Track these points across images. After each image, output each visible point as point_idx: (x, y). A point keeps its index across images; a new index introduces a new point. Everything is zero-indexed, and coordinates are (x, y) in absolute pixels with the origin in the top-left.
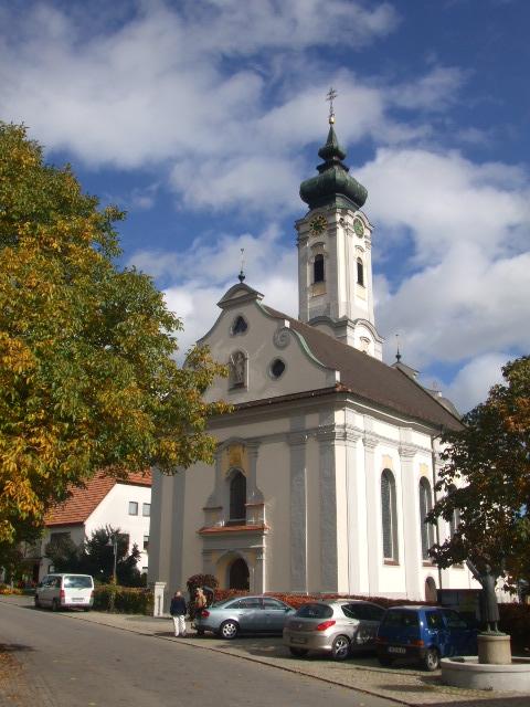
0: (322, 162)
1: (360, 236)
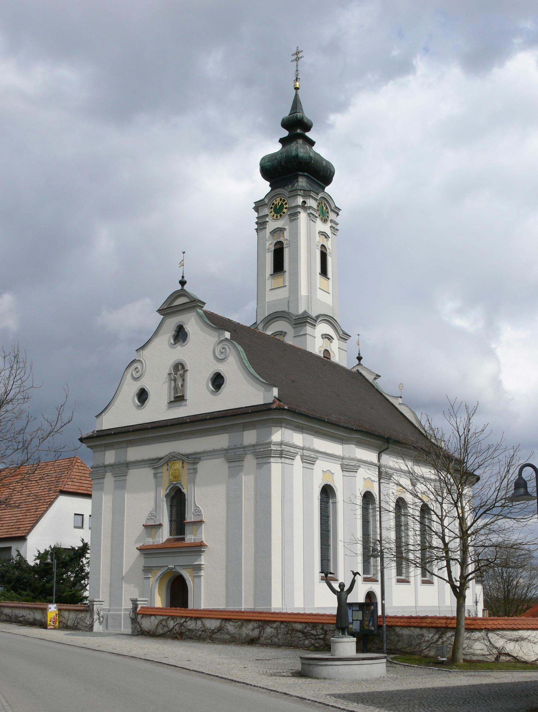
0: (285, 133)
1: (325, 221)
